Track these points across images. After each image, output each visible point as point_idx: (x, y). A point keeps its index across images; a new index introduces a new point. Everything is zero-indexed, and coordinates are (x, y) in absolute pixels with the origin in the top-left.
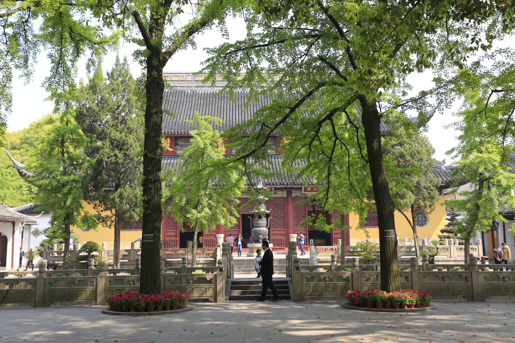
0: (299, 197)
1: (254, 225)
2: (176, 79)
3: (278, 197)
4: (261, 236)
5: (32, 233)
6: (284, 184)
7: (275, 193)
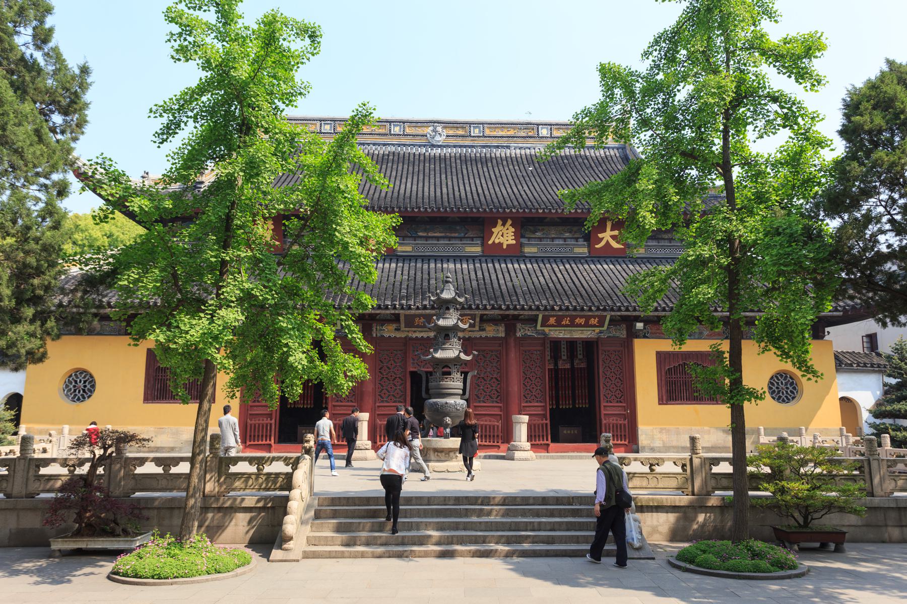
1: (431, 391)
4: (448, 420)
6: (500, 308)
7: (482, 329)
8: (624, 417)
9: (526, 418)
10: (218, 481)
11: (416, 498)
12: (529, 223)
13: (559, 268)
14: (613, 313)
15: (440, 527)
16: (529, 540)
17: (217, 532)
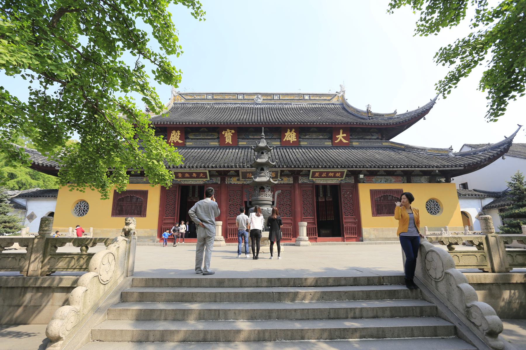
0: (306, 184)
2: (199, 97)
3: (284, 184)
5: (28, 217)
8: (355, 223)
9: (306, 224)
10: (42, 262)
11: (229, 280)
12: (303, 130)
13: (318, 151)
14: (349, 169)
15: (252, 316)
16: (358, 334)
17: (34, 312)
